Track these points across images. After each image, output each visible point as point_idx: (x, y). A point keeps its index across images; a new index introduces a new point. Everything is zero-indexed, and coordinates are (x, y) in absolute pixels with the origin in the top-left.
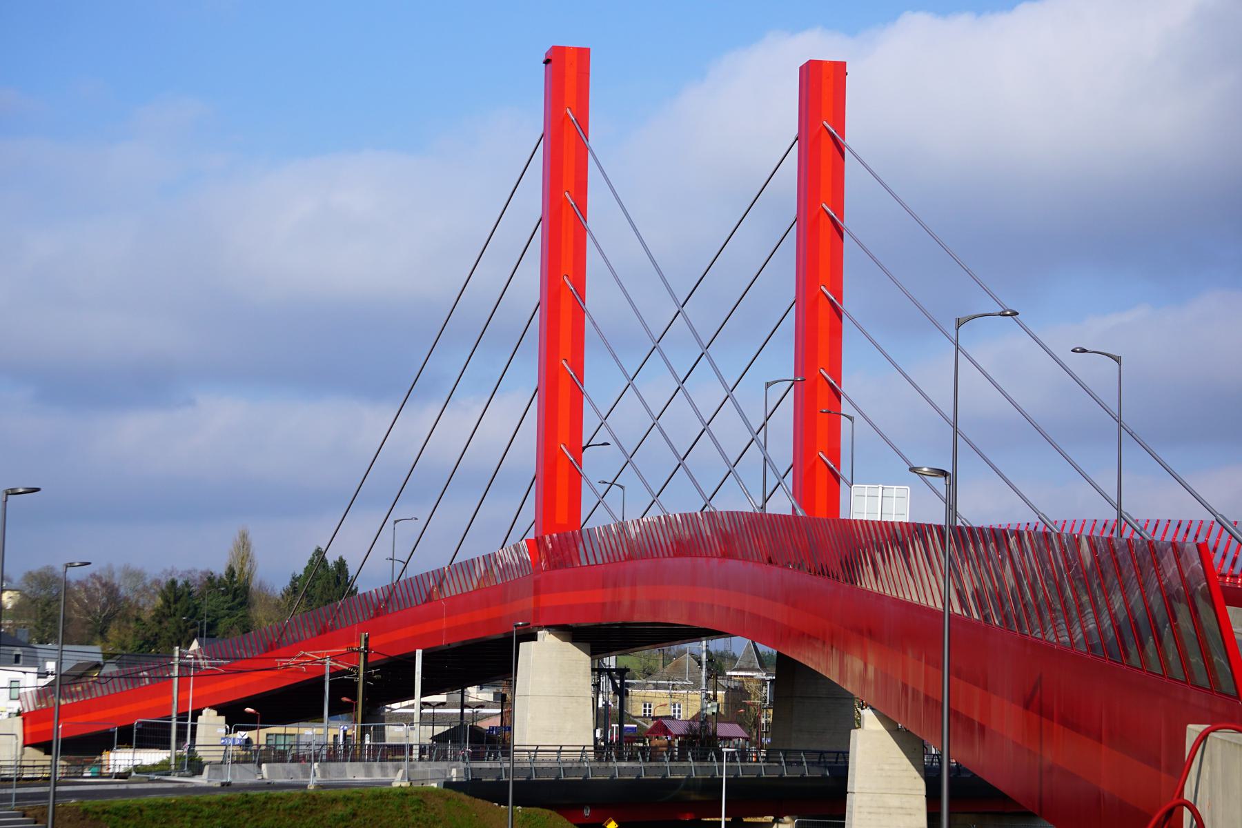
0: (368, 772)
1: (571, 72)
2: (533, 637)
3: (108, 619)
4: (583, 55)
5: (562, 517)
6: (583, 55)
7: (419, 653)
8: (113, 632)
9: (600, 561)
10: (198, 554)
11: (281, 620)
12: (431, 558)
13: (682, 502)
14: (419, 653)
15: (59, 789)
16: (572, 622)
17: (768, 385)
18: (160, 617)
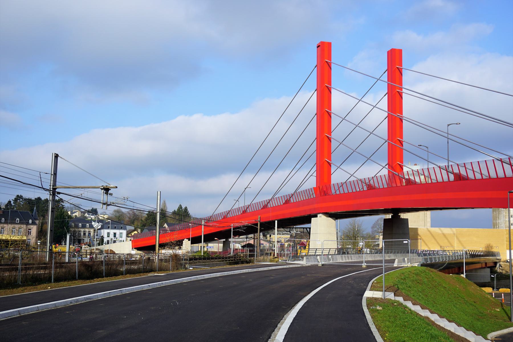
0: (389, 257)
1: (326, 49)
2: (316, 216)
3: (134, 220)
4: (330, 44)
5: (326, 181)
6: (330, 44)
7: (276, 221)
8: (136, 223)
9: (307, 198)
10: (154, 206)
11: (77, 240)
12: (289, 190)
13: (242, 204)
14: (276, 221)
15: (319, 261)
16: (330, 212)
17: (448, 125)
18: (147, 219)
